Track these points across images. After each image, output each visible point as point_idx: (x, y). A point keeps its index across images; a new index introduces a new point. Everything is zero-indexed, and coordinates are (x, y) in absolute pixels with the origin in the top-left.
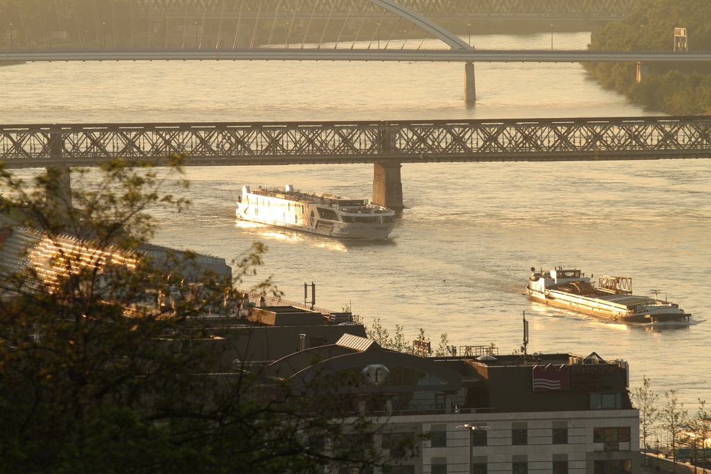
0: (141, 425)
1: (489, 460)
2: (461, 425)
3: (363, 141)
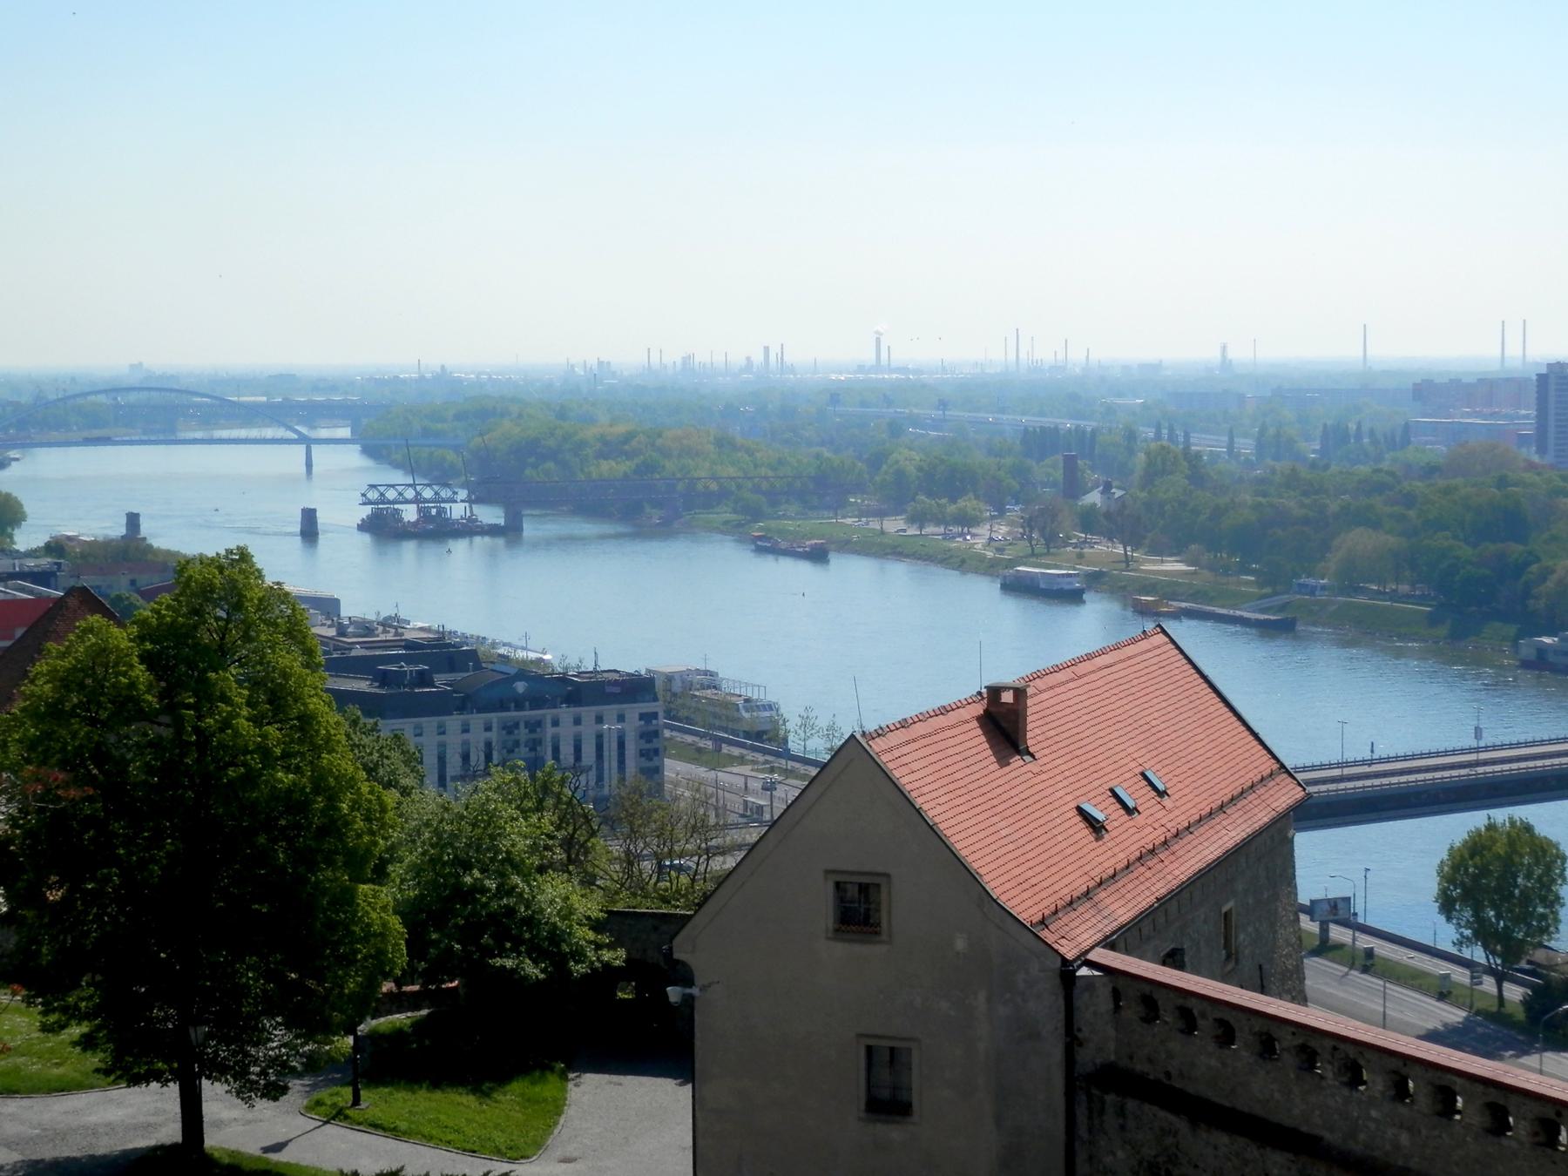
0: (1144, 494)
2: (566, 713)
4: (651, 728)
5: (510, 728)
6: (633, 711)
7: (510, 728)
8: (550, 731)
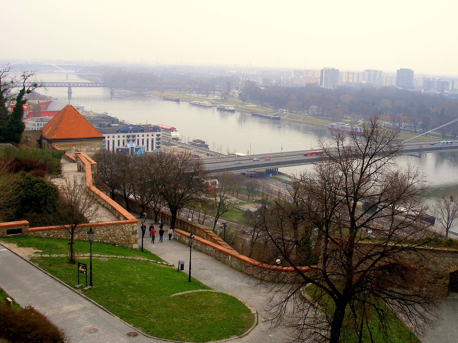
2: (141, 134)
4: (159, 138)
5: (128, 137)
7: (128, 137)
8: (137, 138)
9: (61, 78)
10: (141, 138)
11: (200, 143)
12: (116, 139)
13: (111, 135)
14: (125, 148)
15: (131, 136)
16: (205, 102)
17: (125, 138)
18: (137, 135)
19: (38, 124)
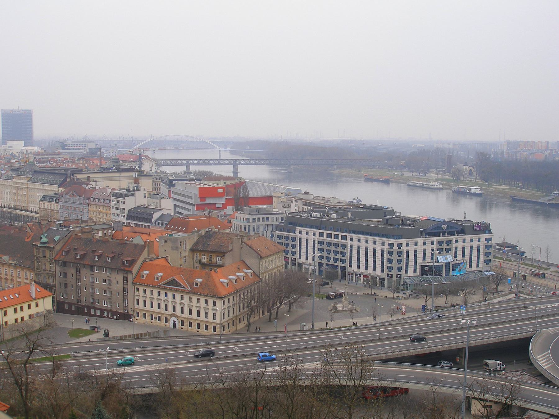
1: (426, 249)
2: (460, 238)
3: (232, 162)
4: (489, 244)
5: (440, 243)
6: (483, 237)
7: (440, 243)
8: (454, 245)
9: (226, 155)
10: (460, 245)
11: (511, 248)
12: (420, 248)
13: (412, 241)
14: (436, 264)
15: (445, 242)
16: (432, 183)
17: (434, 247)
18: (454, 239)
19: (254, 219)
